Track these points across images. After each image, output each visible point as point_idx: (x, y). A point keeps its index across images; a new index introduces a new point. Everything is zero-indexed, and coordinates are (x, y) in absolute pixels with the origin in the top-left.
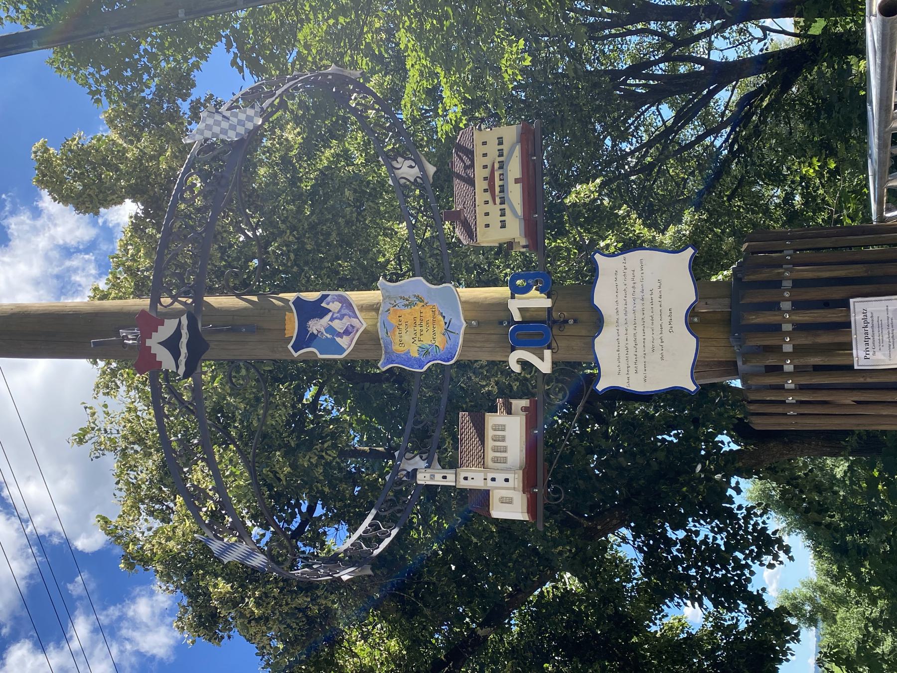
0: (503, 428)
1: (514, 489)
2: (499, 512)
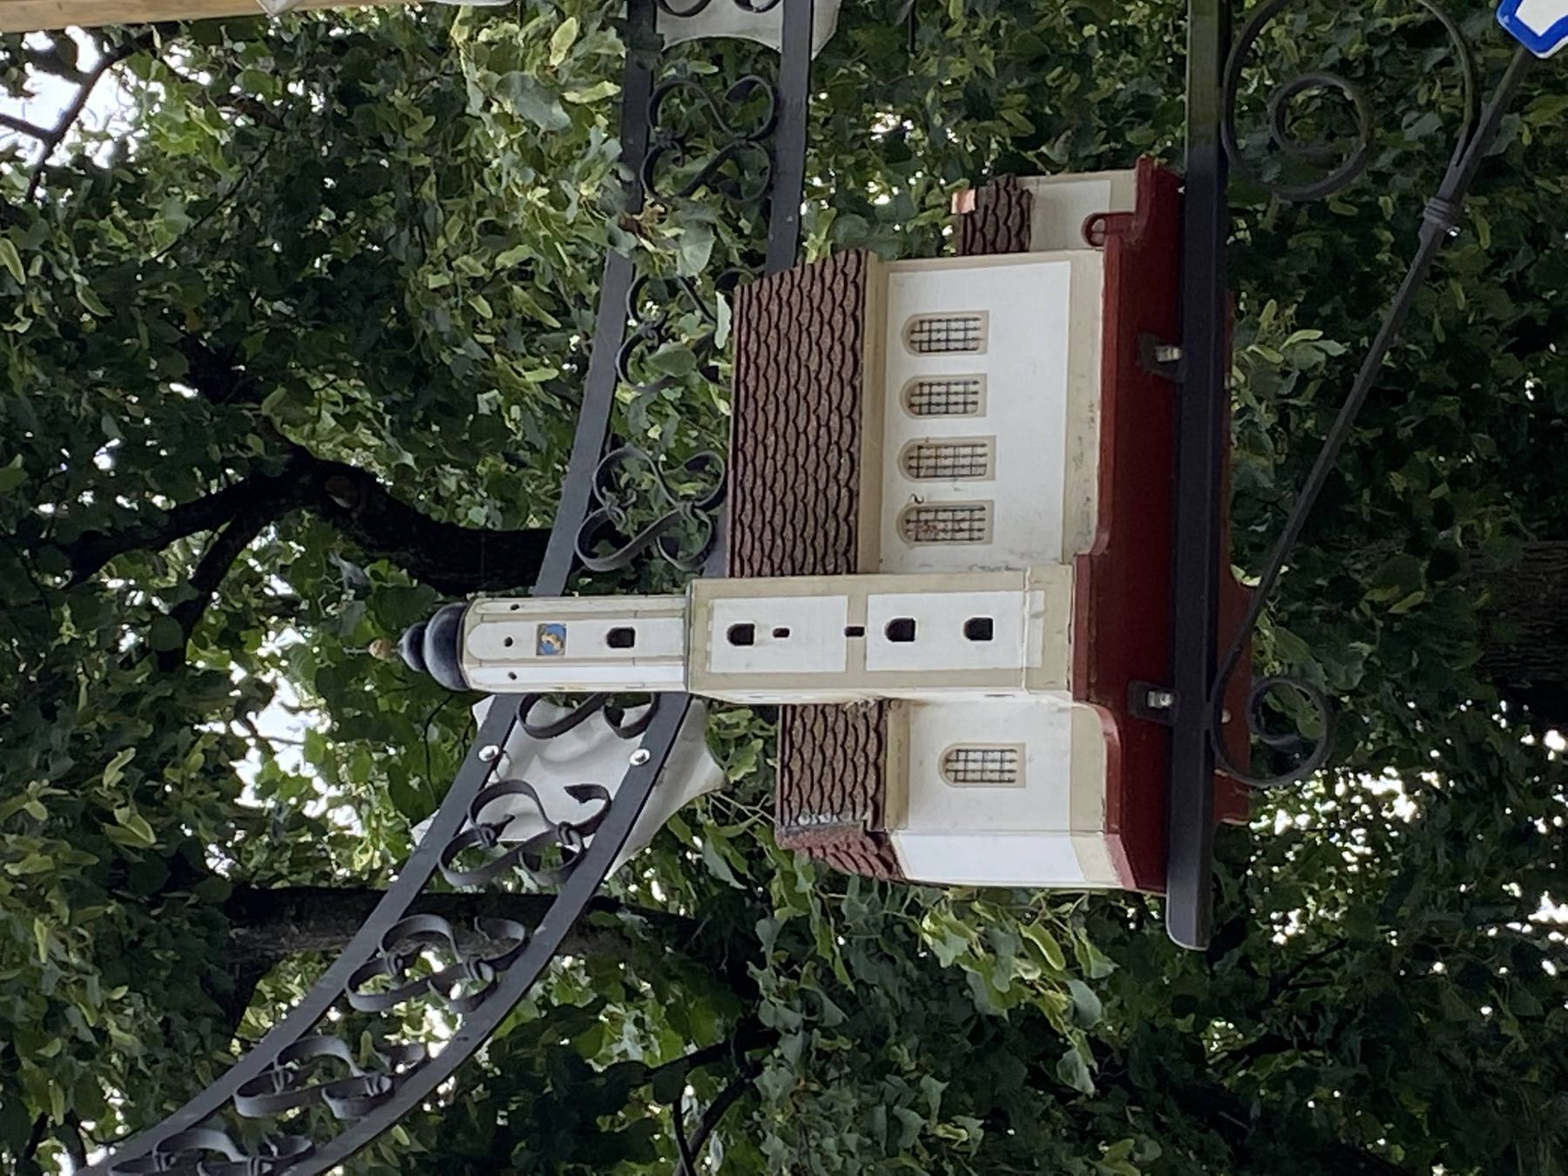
0: (959, 335)
1: (1032, 679)
2: (940, 849)
